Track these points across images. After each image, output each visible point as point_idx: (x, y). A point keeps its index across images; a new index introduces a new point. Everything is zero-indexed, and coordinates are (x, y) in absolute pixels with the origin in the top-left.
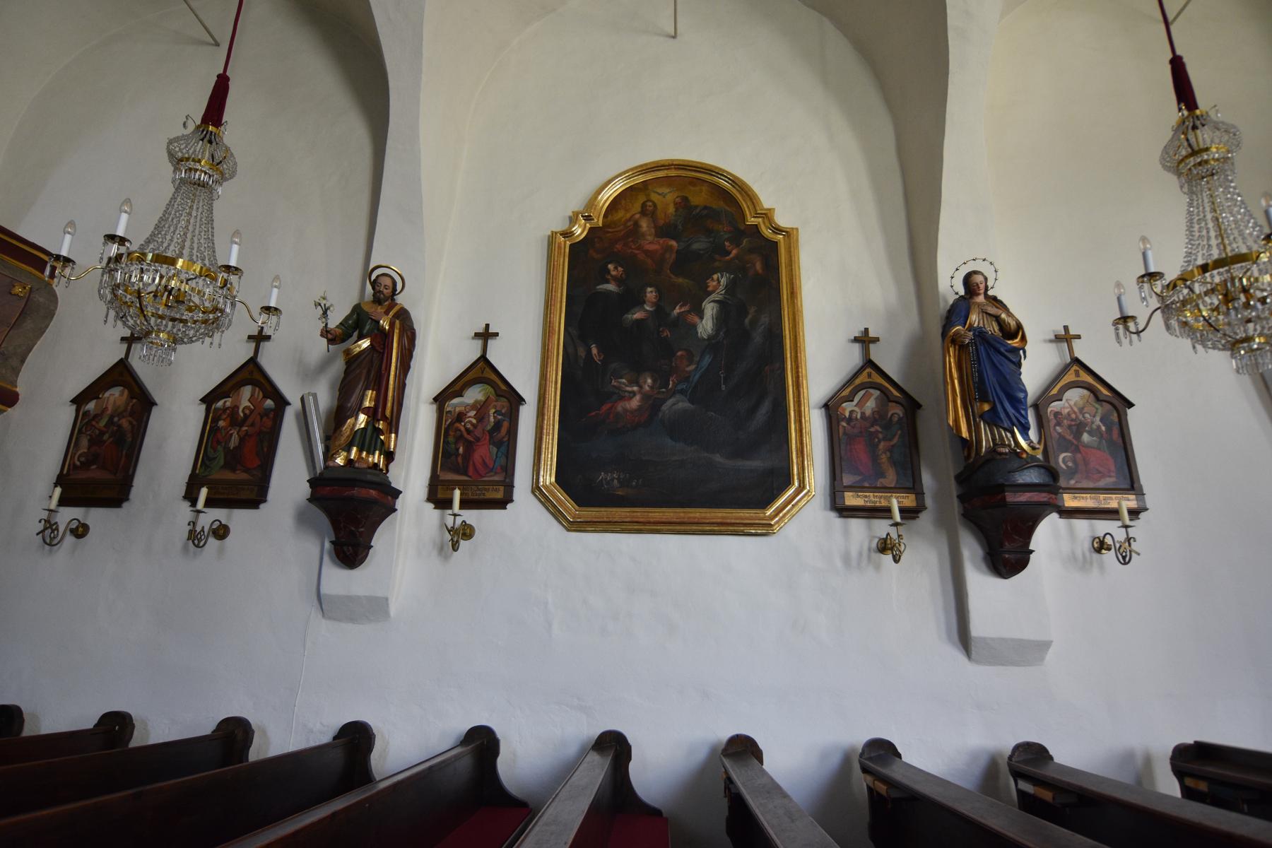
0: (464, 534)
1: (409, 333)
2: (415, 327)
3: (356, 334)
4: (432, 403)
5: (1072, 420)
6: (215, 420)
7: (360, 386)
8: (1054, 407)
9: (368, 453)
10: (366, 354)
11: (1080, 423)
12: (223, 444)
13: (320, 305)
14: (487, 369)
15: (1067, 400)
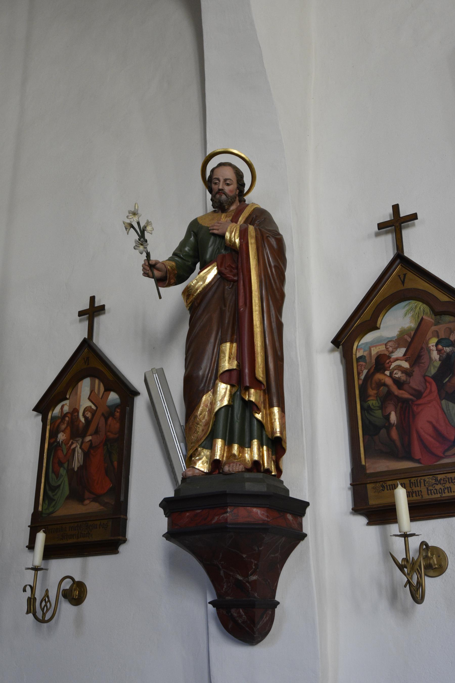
0: (429, 567)
1: (273, 242)
2: (281, 232)
3: (198, 265)
4: (332, 351)
6: (54, 434)
7: (212, 340)
9: (242, 446)
10: (214, 288)
12: (66, 465)
13: (132, 226)
14: (410, 275)
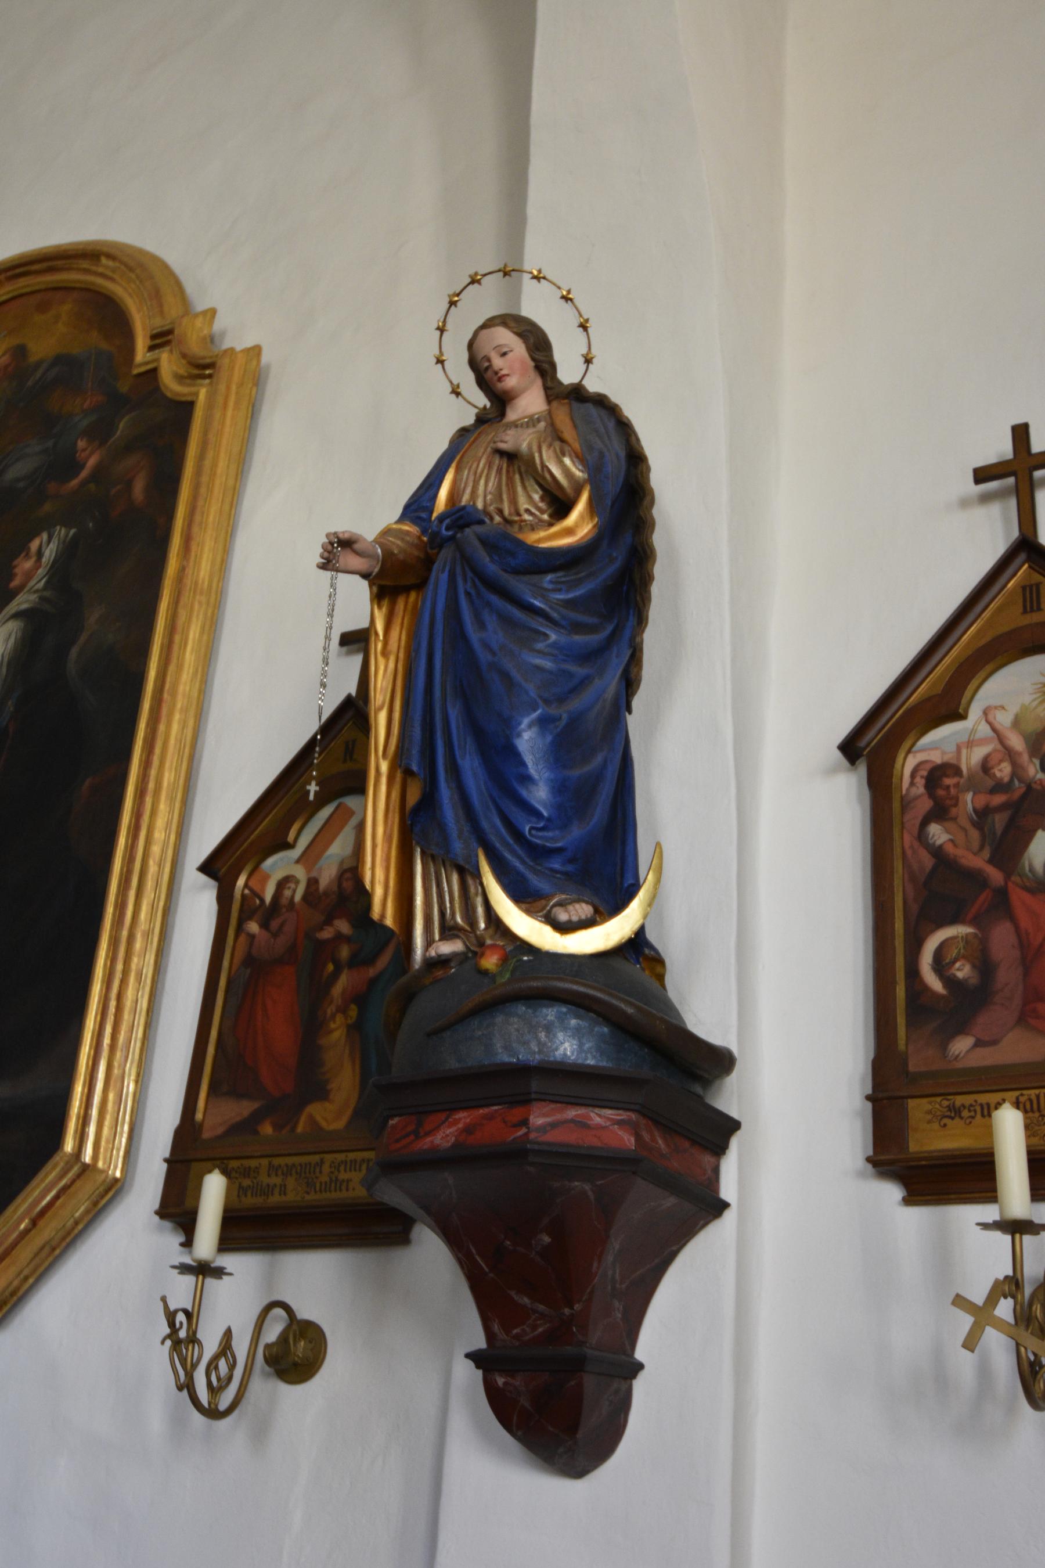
5: (999, 787)
8: (933, 747)
11: (1024, 797)
15: (985, 713)
